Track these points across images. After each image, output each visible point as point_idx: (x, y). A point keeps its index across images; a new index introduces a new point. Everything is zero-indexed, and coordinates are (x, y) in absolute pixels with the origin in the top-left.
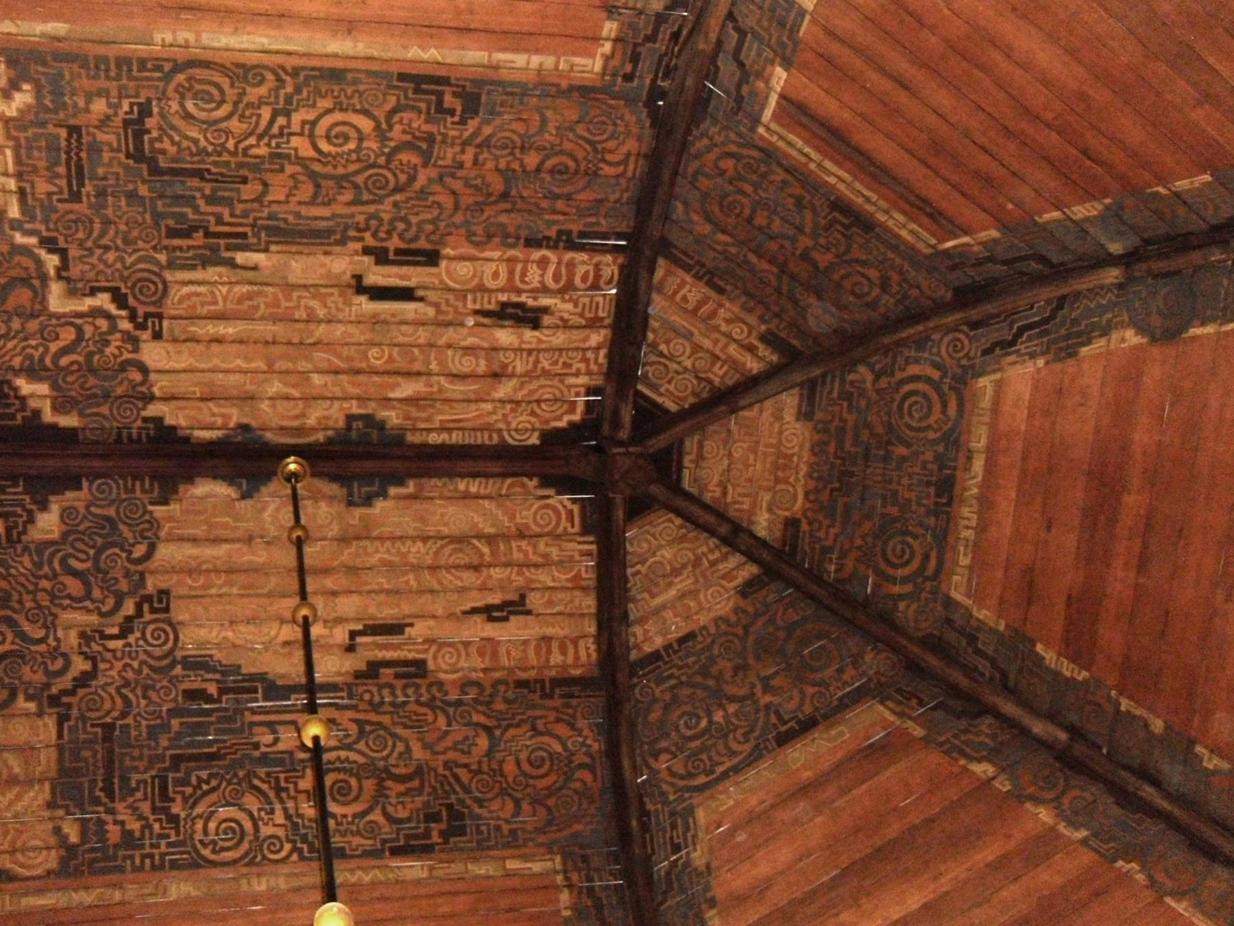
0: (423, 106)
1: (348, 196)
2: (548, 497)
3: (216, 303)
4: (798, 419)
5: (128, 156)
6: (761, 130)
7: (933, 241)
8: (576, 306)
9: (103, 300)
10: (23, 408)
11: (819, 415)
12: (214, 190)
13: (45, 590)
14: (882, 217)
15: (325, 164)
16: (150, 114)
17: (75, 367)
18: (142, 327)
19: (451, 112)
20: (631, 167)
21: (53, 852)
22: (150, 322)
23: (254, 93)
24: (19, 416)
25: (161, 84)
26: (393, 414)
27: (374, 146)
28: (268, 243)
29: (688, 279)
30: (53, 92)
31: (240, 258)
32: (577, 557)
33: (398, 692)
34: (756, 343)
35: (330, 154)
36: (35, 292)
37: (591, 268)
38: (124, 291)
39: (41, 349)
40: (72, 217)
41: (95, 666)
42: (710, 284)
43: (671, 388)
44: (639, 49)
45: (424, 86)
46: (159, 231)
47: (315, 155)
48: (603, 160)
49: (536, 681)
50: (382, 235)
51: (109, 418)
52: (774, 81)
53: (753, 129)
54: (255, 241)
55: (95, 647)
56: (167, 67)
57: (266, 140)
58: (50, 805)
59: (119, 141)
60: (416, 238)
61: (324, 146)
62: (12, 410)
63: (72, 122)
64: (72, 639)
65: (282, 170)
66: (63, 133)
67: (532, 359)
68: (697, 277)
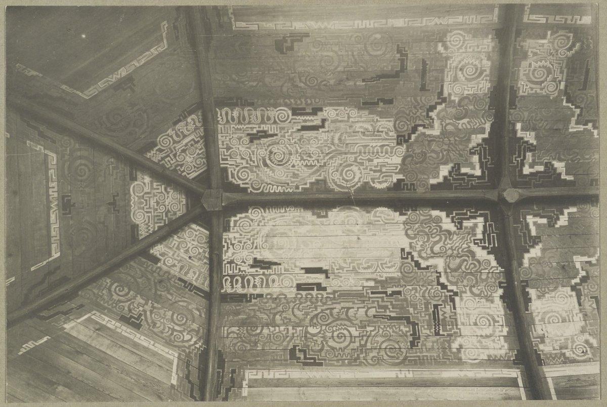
0: (311, 353)
1: (335, 311)
2: (243, 184)
3: (381, 264)
4: (138, 225)
5: (417, 324)
6: (176, 355)
7: (93, 317)
8: (240, 269)
9: (424, 264)
10: (453, 218)
11: (129, 228)
12: (385, 311)
13: (446, 145)
14: (118, 324)
15: (345, 325)
16: (410, 342)
17: (433, 236)
18: (409, 253)
19: (300, 351)
20: (226, 332)
21: (448, 40)
22: (405, 255)
23: (374, 353)
24: (454, 215)
25: (408, 355)
26: (309, 219)
27: (327, 334)
28: (363, 290)
29: (194, 283)
30: (445, 348)
31: (372, 284)
32: (229, 158)
33: (304, 102)
34: (160, 257)
35: (344, 330)
36: (449, 267)
37: (235, 286)
38: (416, 268)
39: (446, 243)
40: (437, 298)
41: (428, 114)
42: (185, 282)
43: (195, 233)
44: (232, 385)
45: (313, 361)
46: (404, 294)
47: (349, 329)
48: (237, 334)
49: (244, 105)
50: (320, 296)
51: (421, 214)
52: (176, 377)
53: (180, 354)
54: (368, 291)
55: (428, 122)
56: (407, 363)
57: (368, 334)
58: (447, 58)
59: (421, 330)
60: (306, 295)
61: (345, 332)
62: (457, 217)
63: (438, 337)
64: (437, 124)
65: (361, 321)
66: (441, 332)
67: (255, 245)
68: (191, 284)
